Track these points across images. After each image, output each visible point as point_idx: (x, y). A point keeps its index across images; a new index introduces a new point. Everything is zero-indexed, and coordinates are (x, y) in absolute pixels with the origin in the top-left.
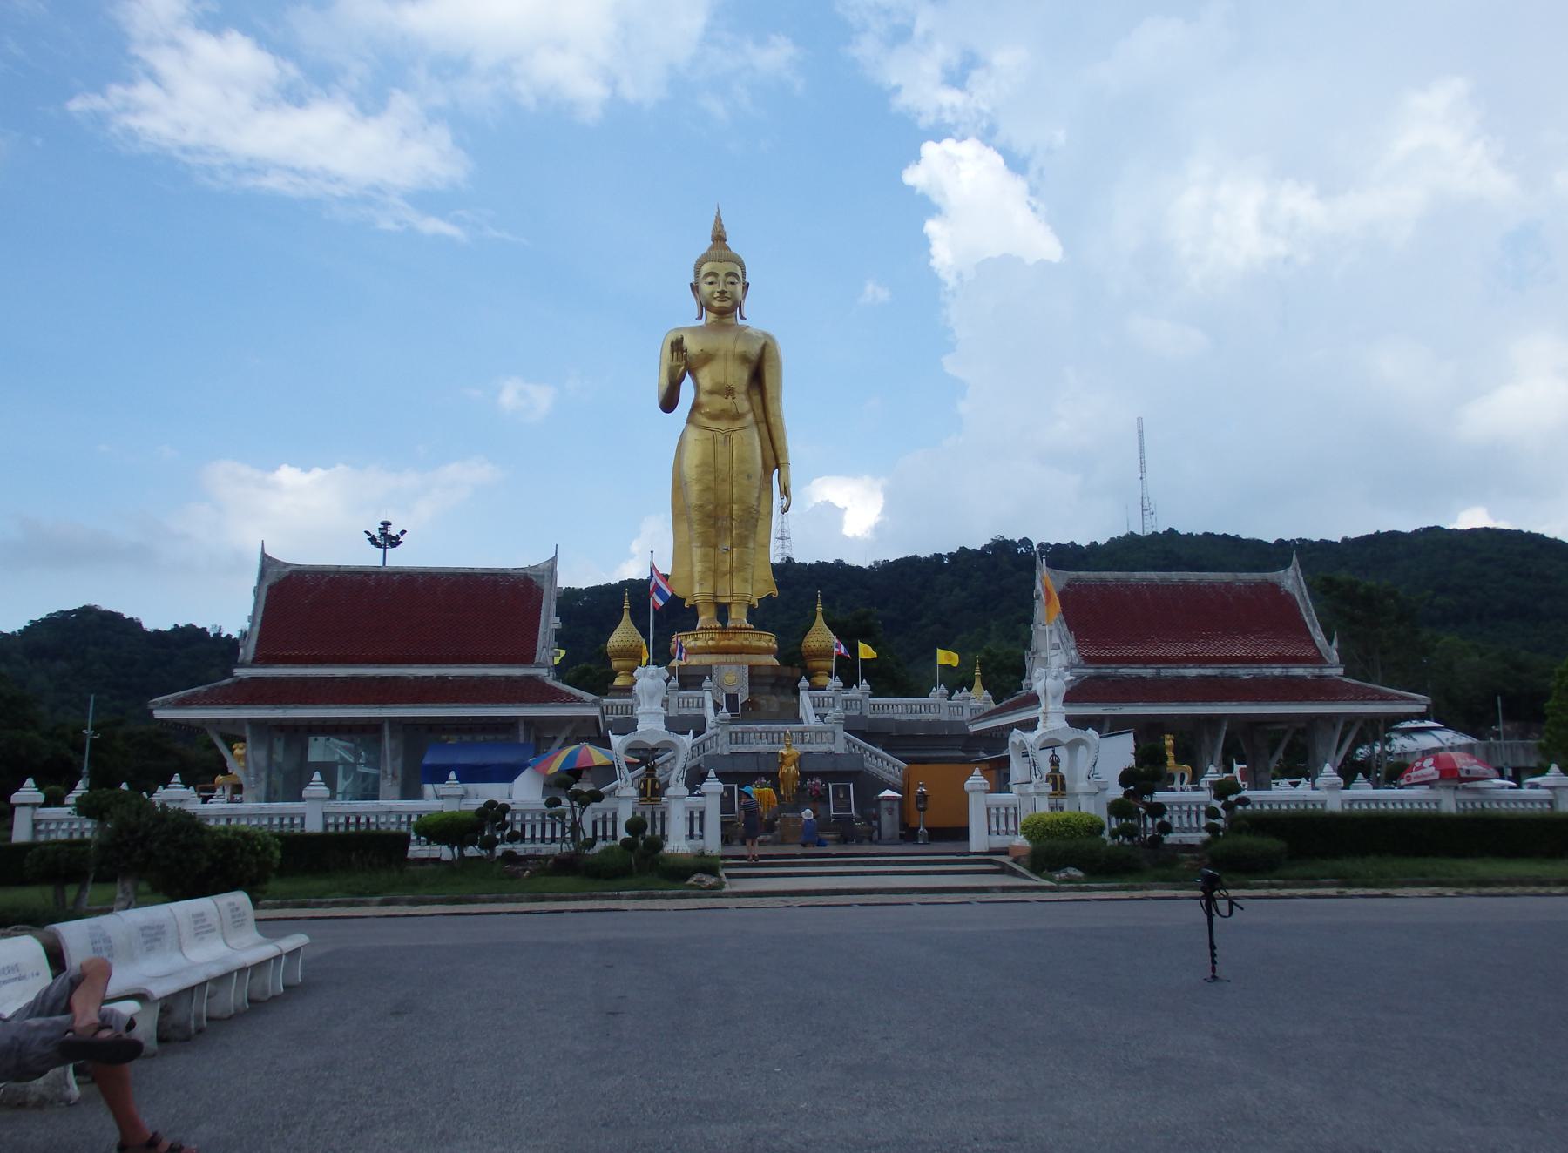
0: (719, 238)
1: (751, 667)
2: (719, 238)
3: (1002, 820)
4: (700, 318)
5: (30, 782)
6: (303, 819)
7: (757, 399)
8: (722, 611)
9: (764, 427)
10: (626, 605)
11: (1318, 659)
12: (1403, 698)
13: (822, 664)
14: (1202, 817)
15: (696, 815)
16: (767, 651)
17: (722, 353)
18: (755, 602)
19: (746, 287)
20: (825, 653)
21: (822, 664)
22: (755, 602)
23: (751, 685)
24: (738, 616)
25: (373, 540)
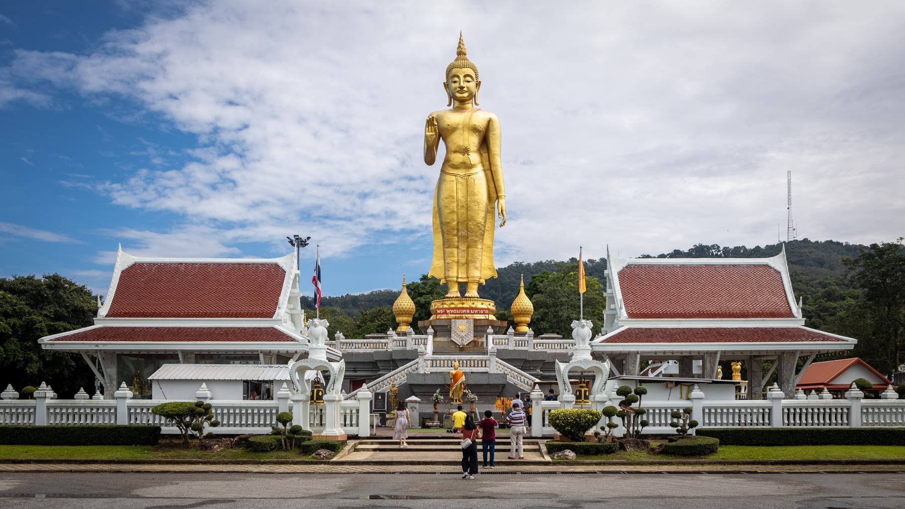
0: (461, 53)
1: (475, 320)
2: (461, 53)
3: (804, 417)
4: (449, 105)
5: (10, 387)
6: (116, 410)
7: (485, 155)
8: (463, 287)
9: (489, 172)
10: (522, 284)
11: (790, 314)
12: (838, 340)
13: (523, 319)
14: (669, 417)
15: (354, 411)
16: (490, 312)
17: (461, 127)
18: (483, 281)
19: (478, 84)
20: (523, 313)
21: (523, 319)
22: (483, 281)
23: (475, 331)
24: (473, 292)
25: (291, 242)
